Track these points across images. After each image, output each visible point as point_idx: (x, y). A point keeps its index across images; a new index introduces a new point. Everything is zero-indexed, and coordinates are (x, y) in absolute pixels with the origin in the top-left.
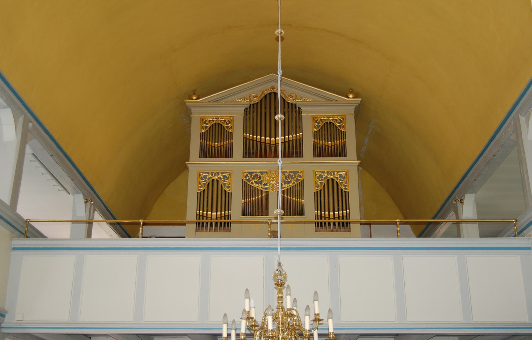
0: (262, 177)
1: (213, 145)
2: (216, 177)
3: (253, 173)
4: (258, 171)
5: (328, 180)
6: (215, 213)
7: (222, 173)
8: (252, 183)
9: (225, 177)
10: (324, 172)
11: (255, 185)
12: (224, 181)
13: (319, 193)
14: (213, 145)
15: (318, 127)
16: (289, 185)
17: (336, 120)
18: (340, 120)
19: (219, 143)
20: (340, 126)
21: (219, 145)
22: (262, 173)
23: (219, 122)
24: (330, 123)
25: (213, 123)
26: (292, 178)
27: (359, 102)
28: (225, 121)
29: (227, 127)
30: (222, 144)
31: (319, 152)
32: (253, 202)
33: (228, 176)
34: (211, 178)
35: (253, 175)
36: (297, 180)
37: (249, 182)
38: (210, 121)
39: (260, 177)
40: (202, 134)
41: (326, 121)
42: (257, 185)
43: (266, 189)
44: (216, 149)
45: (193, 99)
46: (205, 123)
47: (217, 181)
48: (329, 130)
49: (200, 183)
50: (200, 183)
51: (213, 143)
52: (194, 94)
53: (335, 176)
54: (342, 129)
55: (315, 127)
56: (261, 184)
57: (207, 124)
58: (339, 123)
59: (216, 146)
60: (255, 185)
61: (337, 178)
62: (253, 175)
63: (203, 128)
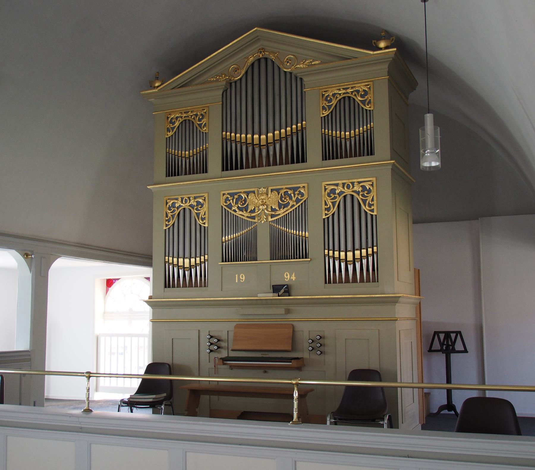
0: (248, 201)
1: (343, 136)
2: (188, 204)
3: (236, 194)
4: (242, 191)
5: (345, 197)
6: (182, 259)
7: (195, 198)
8: (235, 211)
9: (198, 203)
10: (337, 185)
11: (239, 213)
12: (197, 209)
13: (330, 219)
14: (343, 136)
15: (329, 107)
16: (285, 209)
17: (358, 91)
18: (364, 91)
19: (352, 132)
20: (363, 102)
21: (353, 135)
22: (248, 193)
23: (189, 118)
24: (349, 97)
25: (181, 120)
26: (291, 198)
27: (392, 55)
28: (196, 115)
29: (200, 125)
30: (357, 133)
31: (332, 152)
32: (236, 239)
33: (201, 200)
34: (180, 206)
35: (236, 197)
36: (298, 201)
37: (231, 209)
38: (177, 118)
39: (245, 200)
40: (168, 140)
41: (342, 96)
42: (241, 213)
43: (253, 218)
44: (348, 143)
45: (381, 49)
46: (171, 122)
47: (352, 196)
48: (347, 109)
49: (167, 216)
50: (167, 216)
51: (343, 133)
52: (157, 79)
53: (356, 188)
54: (367, 107)
55: (324, 108)
56: (246, 211)
57: (330, 101)
58: (362, 96)
59: (348, 137)
60: (239, 213)
61: (358, 193)
62: (236, 197)
63: (168, 130)
